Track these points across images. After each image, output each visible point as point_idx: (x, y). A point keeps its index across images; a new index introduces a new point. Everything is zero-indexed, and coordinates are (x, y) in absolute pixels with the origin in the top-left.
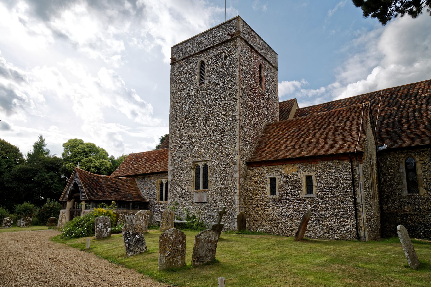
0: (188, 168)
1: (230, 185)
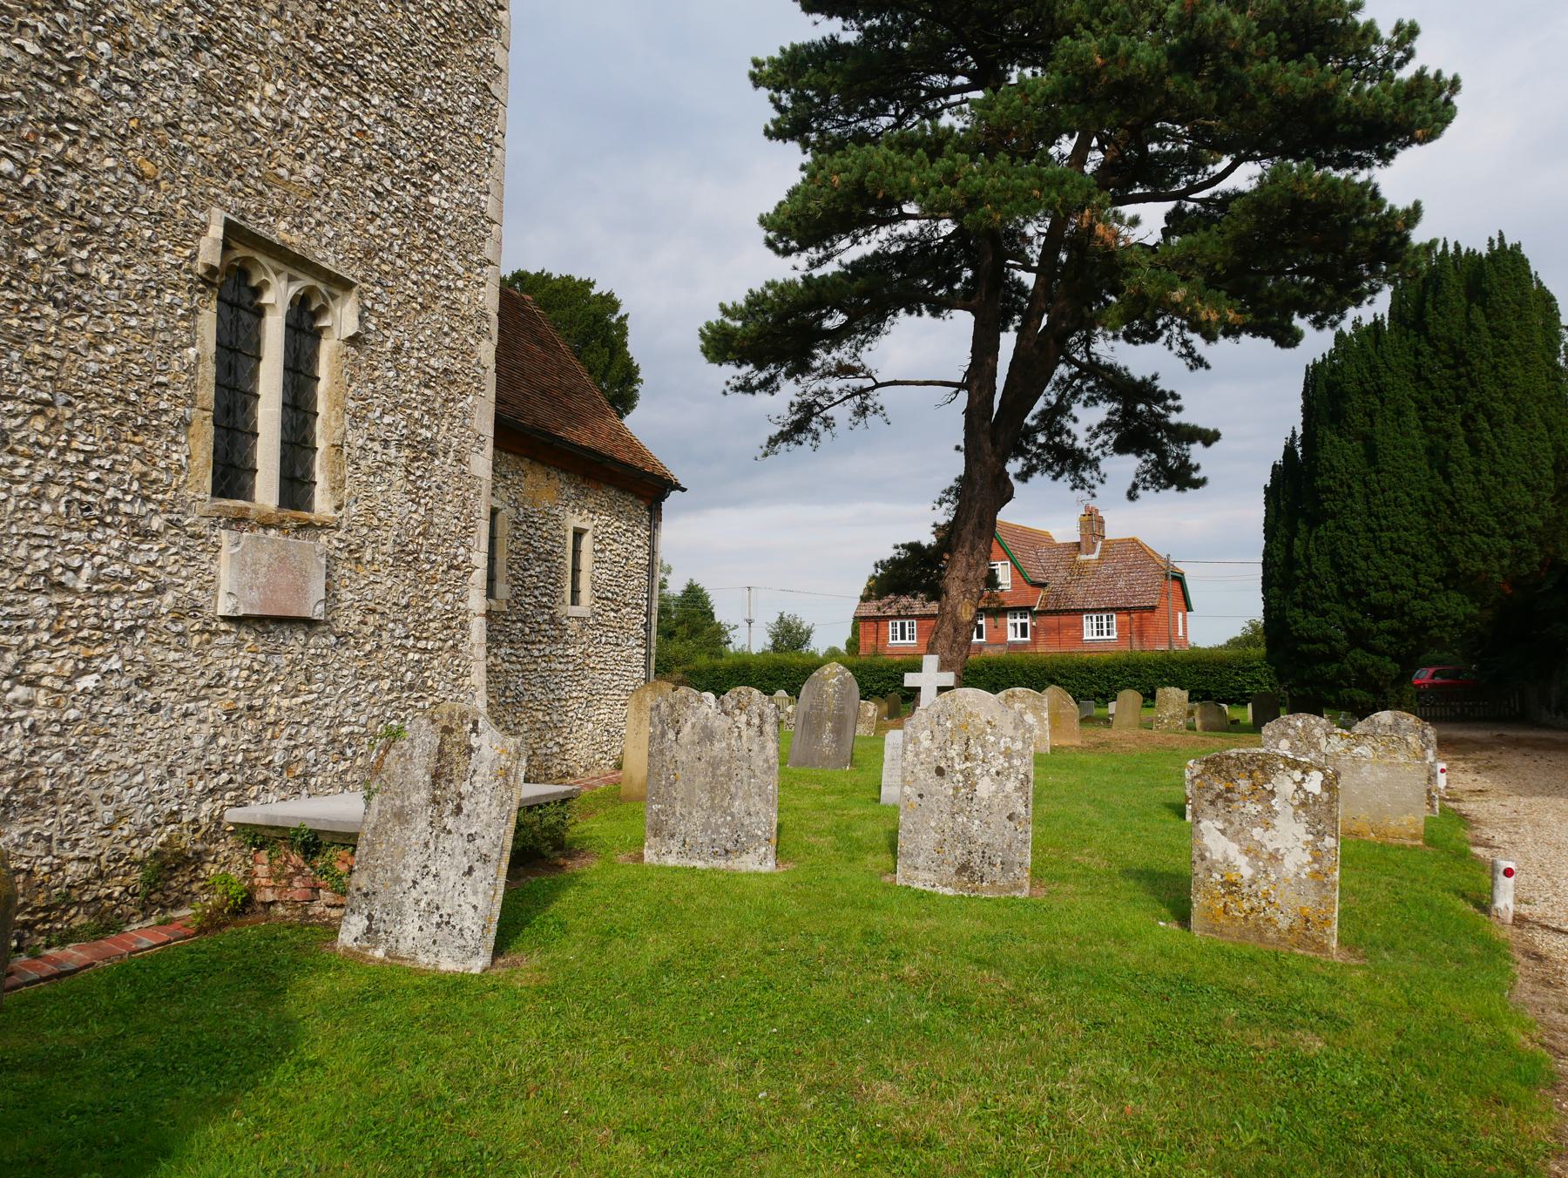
1: (445, 520)
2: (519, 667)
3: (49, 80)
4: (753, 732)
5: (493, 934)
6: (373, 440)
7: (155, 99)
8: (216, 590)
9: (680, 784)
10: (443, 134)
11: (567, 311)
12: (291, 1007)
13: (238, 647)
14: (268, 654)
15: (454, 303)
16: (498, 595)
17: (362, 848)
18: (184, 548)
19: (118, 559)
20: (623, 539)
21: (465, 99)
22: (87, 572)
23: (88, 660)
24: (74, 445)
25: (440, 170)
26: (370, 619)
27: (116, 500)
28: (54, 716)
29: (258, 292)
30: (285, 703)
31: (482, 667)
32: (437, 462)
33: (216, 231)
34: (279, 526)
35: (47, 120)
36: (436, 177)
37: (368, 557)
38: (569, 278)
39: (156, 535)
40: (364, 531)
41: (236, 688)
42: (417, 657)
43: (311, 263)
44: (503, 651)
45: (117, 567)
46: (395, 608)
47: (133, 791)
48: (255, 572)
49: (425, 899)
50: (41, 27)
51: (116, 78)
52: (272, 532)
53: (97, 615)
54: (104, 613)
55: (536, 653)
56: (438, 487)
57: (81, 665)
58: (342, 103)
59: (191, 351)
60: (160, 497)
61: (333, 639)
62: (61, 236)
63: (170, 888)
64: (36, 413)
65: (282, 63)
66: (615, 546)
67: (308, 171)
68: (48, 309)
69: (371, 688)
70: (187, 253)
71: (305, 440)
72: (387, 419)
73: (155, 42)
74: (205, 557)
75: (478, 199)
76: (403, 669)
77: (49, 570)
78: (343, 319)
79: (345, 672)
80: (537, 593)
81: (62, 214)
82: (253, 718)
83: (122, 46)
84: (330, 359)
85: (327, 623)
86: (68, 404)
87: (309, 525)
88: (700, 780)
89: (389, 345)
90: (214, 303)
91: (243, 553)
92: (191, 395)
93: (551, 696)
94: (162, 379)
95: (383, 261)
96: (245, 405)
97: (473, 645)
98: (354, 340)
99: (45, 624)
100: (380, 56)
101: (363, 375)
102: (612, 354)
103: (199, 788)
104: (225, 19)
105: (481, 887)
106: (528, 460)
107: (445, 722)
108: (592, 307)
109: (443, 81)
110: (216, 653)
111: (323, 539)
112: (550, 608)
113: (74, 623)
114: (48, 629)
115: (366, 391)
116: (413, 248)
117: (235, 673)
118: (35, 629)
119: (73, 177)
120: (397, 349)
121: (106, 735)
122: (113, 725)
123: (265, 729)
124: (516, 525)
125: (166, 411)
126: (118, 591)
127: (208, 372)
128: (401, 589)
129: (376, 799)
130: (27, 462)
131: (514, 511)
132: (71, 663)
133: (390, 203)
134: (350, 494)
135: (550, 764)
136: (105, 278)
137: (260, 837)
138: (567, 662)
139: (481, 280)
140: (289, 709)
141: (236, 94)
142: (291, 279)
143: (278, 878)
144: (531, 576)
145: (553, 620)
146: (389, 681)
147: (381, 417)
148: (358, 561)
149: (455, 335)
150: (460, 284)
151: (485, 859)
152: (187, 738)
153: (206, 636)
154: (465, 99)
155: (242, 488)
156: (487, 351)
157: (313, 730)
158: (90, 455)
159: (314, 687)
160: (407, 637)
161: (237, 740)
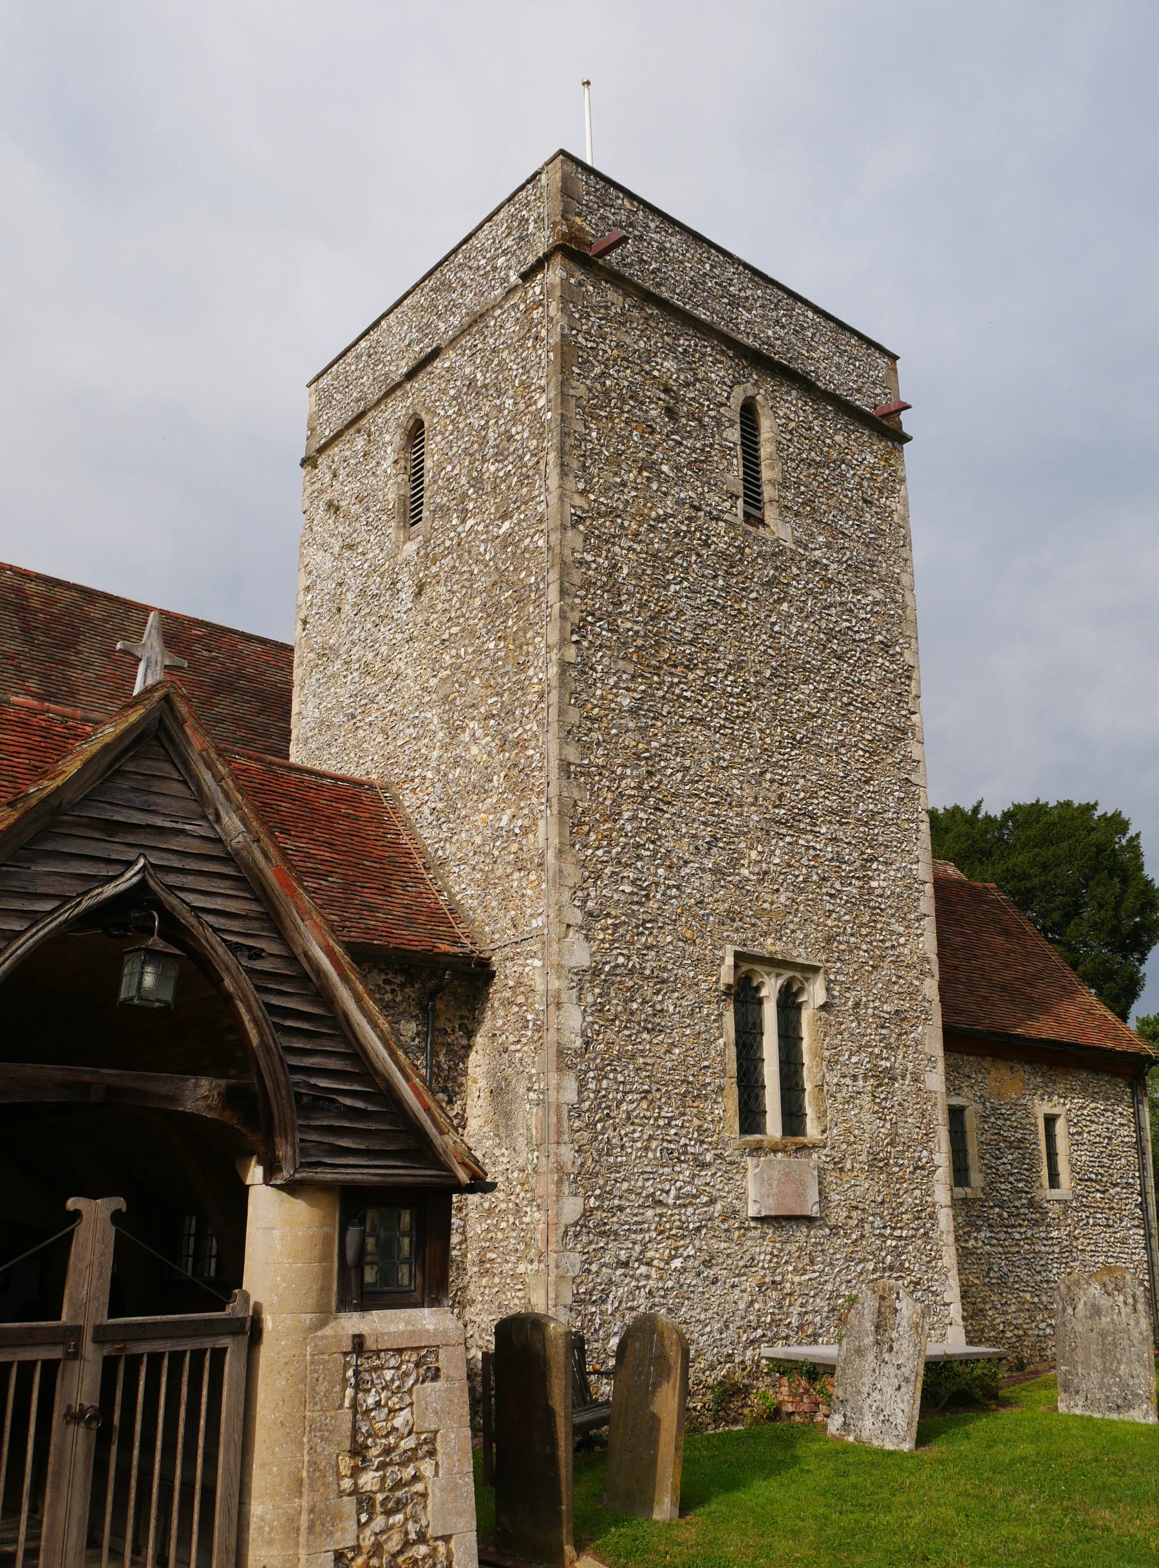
0: (703, 986)
1: (909, 1127)
2: (1000, 1249)
3: (637, 903)
4: (1129, 1310)
5: (915, 1429)
6: (845, 1077)
7: (689, 891)
8: (746, 1199)
9: (1079, 1350)
10: (876, 831)
11: (1065, 845)
12: (799, 1452)
13: (763, 1238)
14: (783, 1243)
15: (898, 956)
16: (973, 1184)
17: (838, 1372)
18: (726, 1172)
19: (689, 1183)
20: (1102, 1120)
21: (891, 798)
22: (673, 1193)
23: (676, 1249)
24: (663, 1114)
25: (876, 859)
26: (854, 1214)
27: (686, 1145)
28: (660, 1285)
29: (758, 989)
30: (797, 1279)
31: (952, 1250)
32: (897, 1085)
33: (730, 960)
34: (784, 1151)
35: (637, 927)
36: (874, 866)
37: (849, 1166)
38: (1068, 804)
39: (709, 1165)
40: (844, 1146)
41: (763, 1268)
42: (894, 1243)
43: (790, 963)
44: (983, 1234)
45: (689, 1188)
46: (873, 1205)
47: (705, 1337)
48: (770, 1185)
49: (875, 1405)
50: (631, 875)
51: (669, 887)
52: (780, 1155)
53: (680, 1220)
54: (683, 1218)
55: (1017, 1236)
56: (900, 1105)
57: (673, 1252)
58: (801, 842)
59: (721, 1041)
60: (710, 1139)
61: (827, 1231)
62: (648, 990)
63: (730, 1409)
64: (642, 1098)
65: (759, 834)
66: (1094, 1127)
67: (782, 899)
68: (645, 1036)
69: (859, 1269)
70: (714, 979)
71: (797, 1084)
72: (854, 1059)
73: (687, 856)
74: (738, 1177)
75: (911, 869)
76: (883, 1254)
77: (654, 1193)
78: (815, 993)
79: (838, 1256)
80: (1011, 1179)
81: (648, 977)
82: (776, 1290)
83: (670, 867)
84: (809, 1023)
85: (822, 1219)
86: (658, 1090)
87: (802, 1148)
88: (1094, 1347)
89: (850, 1003)
90: (732, 1006)
91: (762, 1172)
92: (723, 1070)
93: (1039, 1278)
94: (706, 1063)
95: (840, 943)
96: (756, 1068)
97: (942, 1232)
98: (825, 1007)
99: (653, 1227)
100: (824, 797)
101: (833, 1031)
102: (1125, 881)
103: (744, 1339)
104: (723, 822)
105: (906, 1398)
106: (990, 1059)
107: (881, 1293)
108: (1094, 836)
109: (873, 792)
110: (749, 1243)
111: (815, 1156)
112: (1027, 1193)
113: (668, 1225)
114: (655, 1230)
115: (837, 1042)
116: (862, 925)
117: (762, 1257)
118: (649, 1230)
119: (652, 954)
120: (857, 1005)
121: (689, 1299)
122: (692, 1292)
123: (784, 1299)
124: (984, 1119)
125: (709, 1084)
126: (691, 1204)
127: (732, 1052)
128: (876, 1189)
129: (845, 1341)
130: (640, 1129)
131: (981, 1106)
132: (667, 1251)
133: (841, 899)
134: (831, 1120)
135: (1044, 1345)
136: (671, 1009)
137: (784, 1367)
138: (1053, 1245)
139: (919, 931)
140: (800, 1284)
141: (734, 867)
142: (778, 975)
143: (795, 1396)
144: (1004, 1164)
145: (1031, 1203)
146: (872, 1263)
147: (850, 1058)
148: (842, 1170)
149: (902, 981)
150: (902, 940)
151: (907, 1380)
152: (735, 1303)
153: (742, 1231)
154: (891, 798)
155: (758, 1125)
156: (930, 988)
157: (818, 1300)
158: (671, 1119)
159: (816, 1268)
160: (885, 1227)
161: (767, 1305)
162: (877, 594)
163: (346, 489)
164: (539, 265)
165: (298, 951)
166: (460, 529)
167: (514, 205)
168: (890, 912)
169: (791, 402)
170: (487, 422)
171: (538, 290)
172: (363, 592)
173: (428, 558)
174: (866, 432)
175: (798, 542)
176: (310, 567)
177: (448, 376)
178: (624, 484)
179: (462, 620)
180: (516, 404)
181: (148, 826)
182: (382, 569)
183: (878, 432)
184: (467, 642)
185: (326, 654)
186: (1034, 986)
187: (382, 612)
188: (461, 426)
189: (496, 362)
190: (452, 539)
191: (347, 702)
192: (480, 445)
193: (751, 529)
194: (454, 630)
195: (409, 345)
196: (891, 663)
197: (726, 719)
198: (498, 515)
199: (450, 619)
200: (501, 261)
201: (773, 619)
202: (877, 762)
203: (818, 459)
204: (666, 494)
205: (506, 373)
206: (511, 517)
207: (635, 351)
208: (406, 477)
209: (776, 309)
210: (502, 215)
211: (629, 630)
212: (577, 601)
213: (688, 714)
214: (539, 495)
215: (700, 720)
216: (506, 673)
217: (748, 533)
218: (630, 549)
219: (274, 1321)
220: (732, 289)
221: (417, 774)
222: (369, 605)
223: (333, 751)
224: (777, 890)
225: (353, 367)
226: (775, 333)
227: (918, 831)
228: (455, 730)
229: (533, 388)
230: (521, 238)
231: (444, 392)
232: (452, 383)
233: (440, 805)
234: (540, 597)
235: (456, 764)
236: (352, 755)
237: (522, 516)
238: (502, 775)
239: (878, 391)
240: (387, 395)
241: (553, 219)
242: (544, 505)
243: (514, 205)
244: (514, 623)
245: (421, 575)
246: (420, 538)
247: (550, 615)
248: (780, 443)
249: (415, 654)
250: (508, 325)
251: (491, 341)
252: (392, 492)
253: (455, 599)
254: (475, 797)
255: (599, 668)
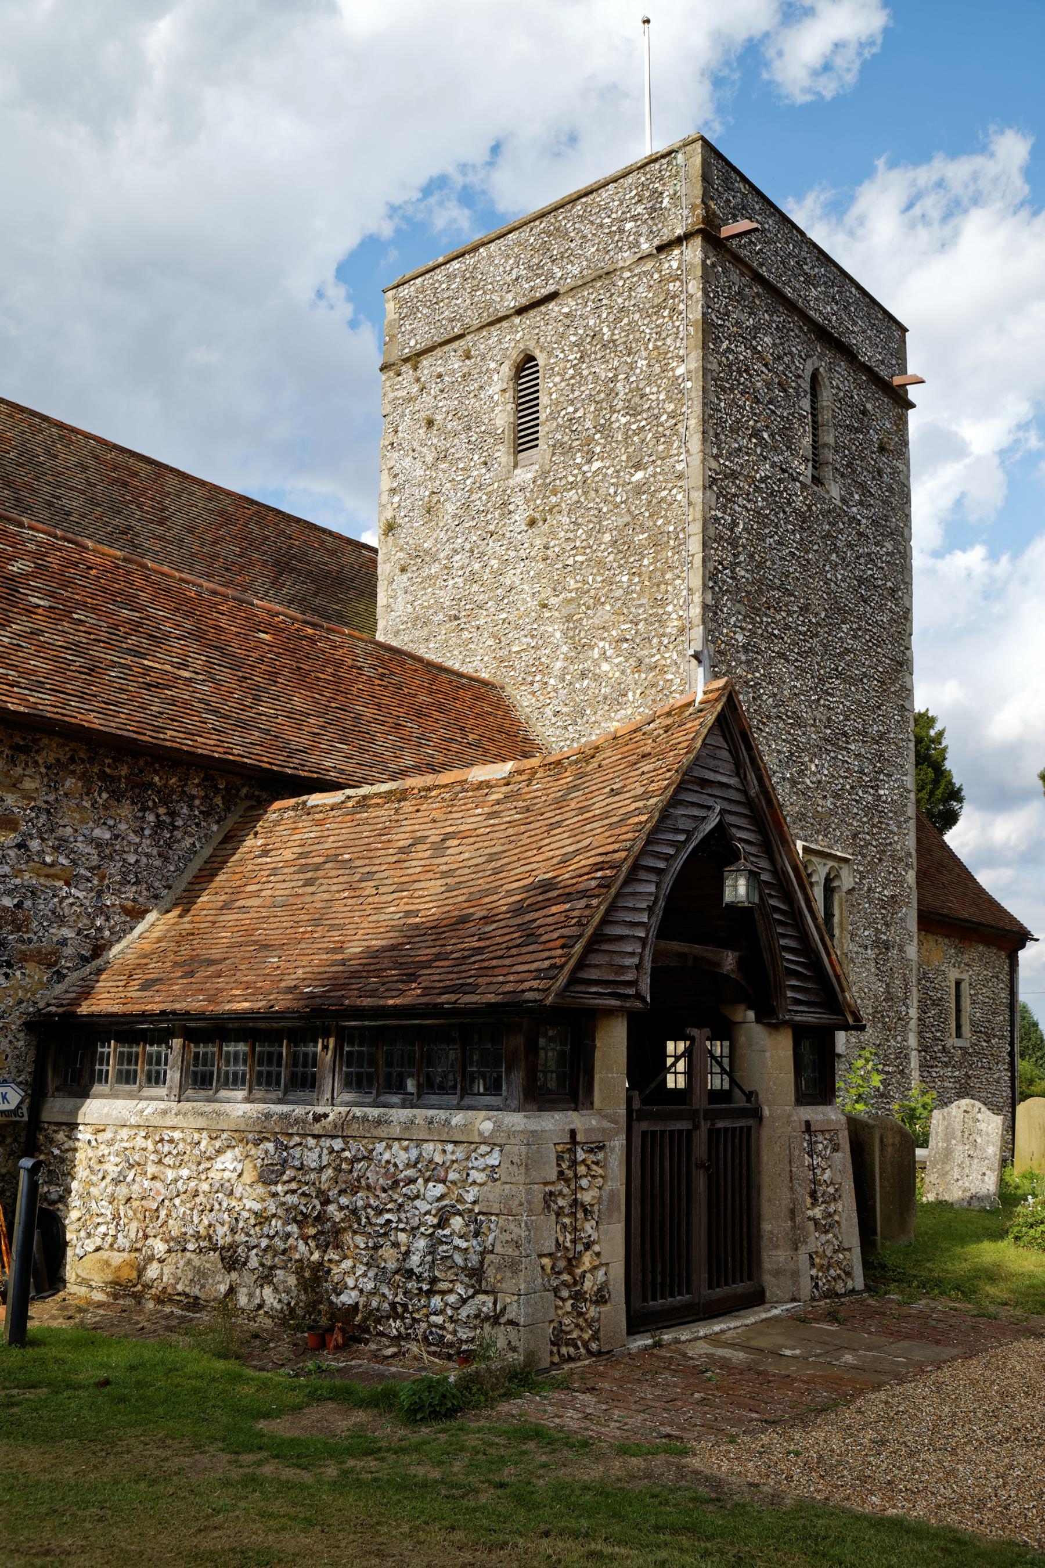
55: (934, 1075)
72: (866, 933)
80: (933, 1029)
116: (873, 826)
150: (896, 838)
156: (911, 877)
162: (889, 546)
163: (441, 404)
164: (679, 241)
165: (779, 867)
166: (585, 468)
167: (645, 174)
168: (891, 815)
169: (839, 373)
170: (616, 376)
171: (675, 264)
172: (466, 506)
173: (545, 484)
174: (886, 400)
175: (843, 500)
176: (396, 470)
177: (567, 322)
178: (740, 449)
179: (588, 551)
180: (649, 366)
181: (719, 782)
182: (490, 489)
183: (894, 399)
184: (595, 571)
185: (420, 556)
186: (941, 873)
187: (491, 528)
188: (585, 373)
189: (626, 321)
190: (576, 476)
191: (448, 603)
192: (608, 395)
193: (816, 488)
194: (579, 558)
195: (517, 279)
196: (896, 605)
197: (798, 653)
198: (631, 464)
199: (575, 548)
200: (629, 226)
201: (827, 568)
202: (885, 691)
203: (856, 425)
204: (765, 458)
205: (637, 335)
206: (646, 469)
207: (748, 327)
208: (513, 406)
209: (833, 286)
210: (630, 180)
211: (743, 577)
212: (712, 552)
213: (777, 649)
214: (679, 454)
215: (784, 654)
216: (641, 605)
217: (814, 493)
218: (744, 507)
219: (770, 1110)
220: (805, 267)
221: (537, 678)
222: (474, 518)
223: (431, 645)
224: (825, 797)
225: (444, 286)
226: (832, 309)
227: (908, 748)
228: (580, 648)
229: (670, 355)
230: (654, 209)
231: (562, 336)
232: (572, 330)
233: (565, 710)
234: (680, 545)
235: (583, 675)
236: (456, 652)
237: (658, 470)
238: (638, 692)
239: (894, 362)
240: (491, 324)
241: (693, 200)
242: (683, 465)
243: (645, 174)
244: (652, 564)
245: (538, 502)
246: (537, 467)
247: (691, 562)
248: (833, 411)
249: (532, 573)
250: (640, 289)
251: (620, 300)
252: (503, 418)
253: (580, 531)
254: (607, 708)
255: (725, 609)
